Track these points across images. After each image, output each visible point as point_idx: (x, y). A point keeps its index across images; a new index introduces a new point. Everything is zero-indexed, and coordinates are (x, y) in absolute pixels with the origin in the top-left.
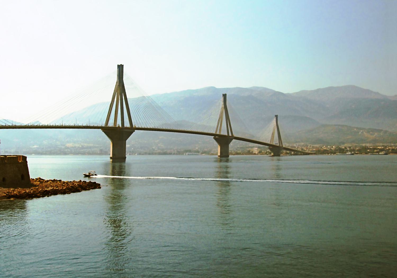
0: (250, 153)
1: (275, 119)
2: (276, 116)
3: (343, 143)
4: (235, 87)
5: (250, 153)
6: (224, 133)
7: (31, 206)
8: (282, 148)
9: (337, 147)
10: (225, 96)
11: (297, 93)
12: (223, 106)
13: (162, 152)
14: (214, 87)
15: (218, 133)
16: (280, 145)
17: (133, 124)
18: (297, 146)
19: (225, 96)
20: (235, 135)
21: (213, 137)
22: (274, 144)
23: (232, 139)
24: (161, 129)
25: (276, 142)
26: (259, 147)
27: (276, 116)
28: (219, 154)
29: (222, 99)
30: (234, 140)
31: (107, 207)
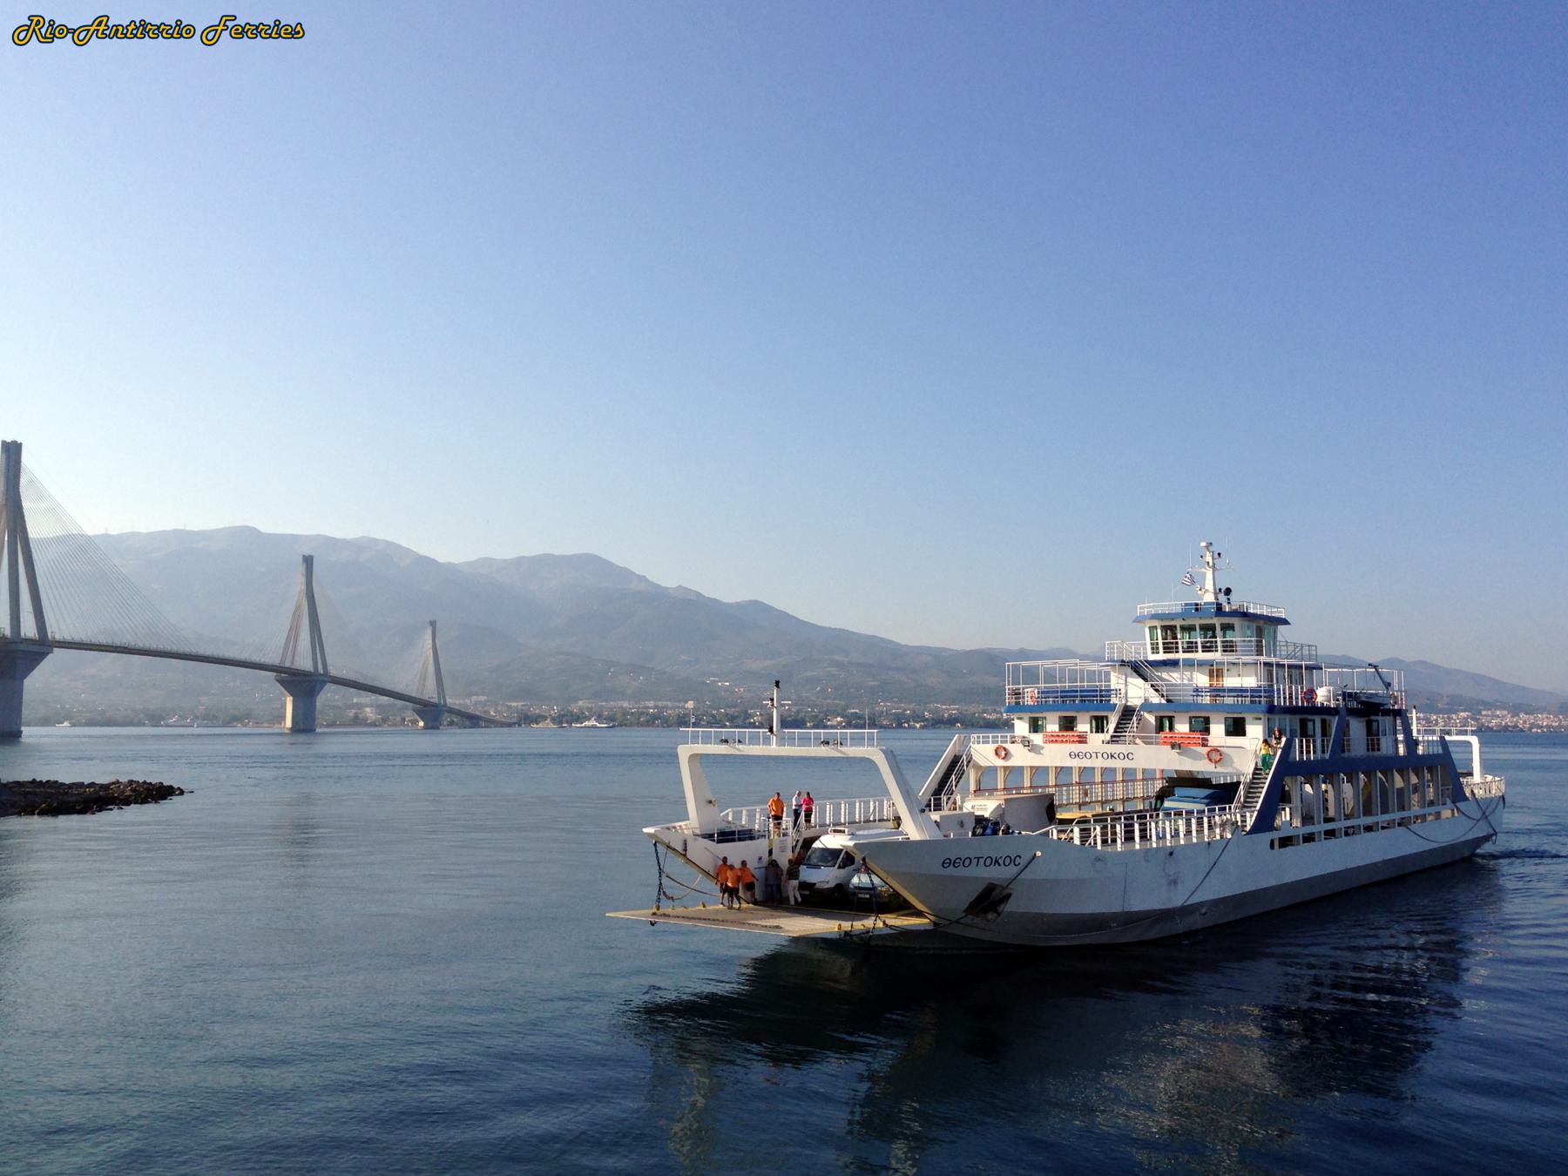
0: (358, 721)
1: (429, 631)
2: (433, 624)
3: (576, 700)
4: (314, 533)
5: (358, 721)
6: (304, 662)
7: (136, 926)
8: (445, 709)
9: (563, 710)
10: (308, 561)
11: (469, 563)
12: (303, 587)
13: (99, 718)
14: (253, 531)
15: (287, 664)
16: (439, 699)
17: (297, 658)
18: (471, 703)
19: (308, 561)
20: (333, 672)
21: (275, 674)
22: (425, 697)
23: (325, 682)
24: (152, 648)
25: (430, 693)
26: (379, 707)
27: (433, 624)
28: (289, 723)
29: (302, 568)
30: (330, 687)
31: (1461, 919)
